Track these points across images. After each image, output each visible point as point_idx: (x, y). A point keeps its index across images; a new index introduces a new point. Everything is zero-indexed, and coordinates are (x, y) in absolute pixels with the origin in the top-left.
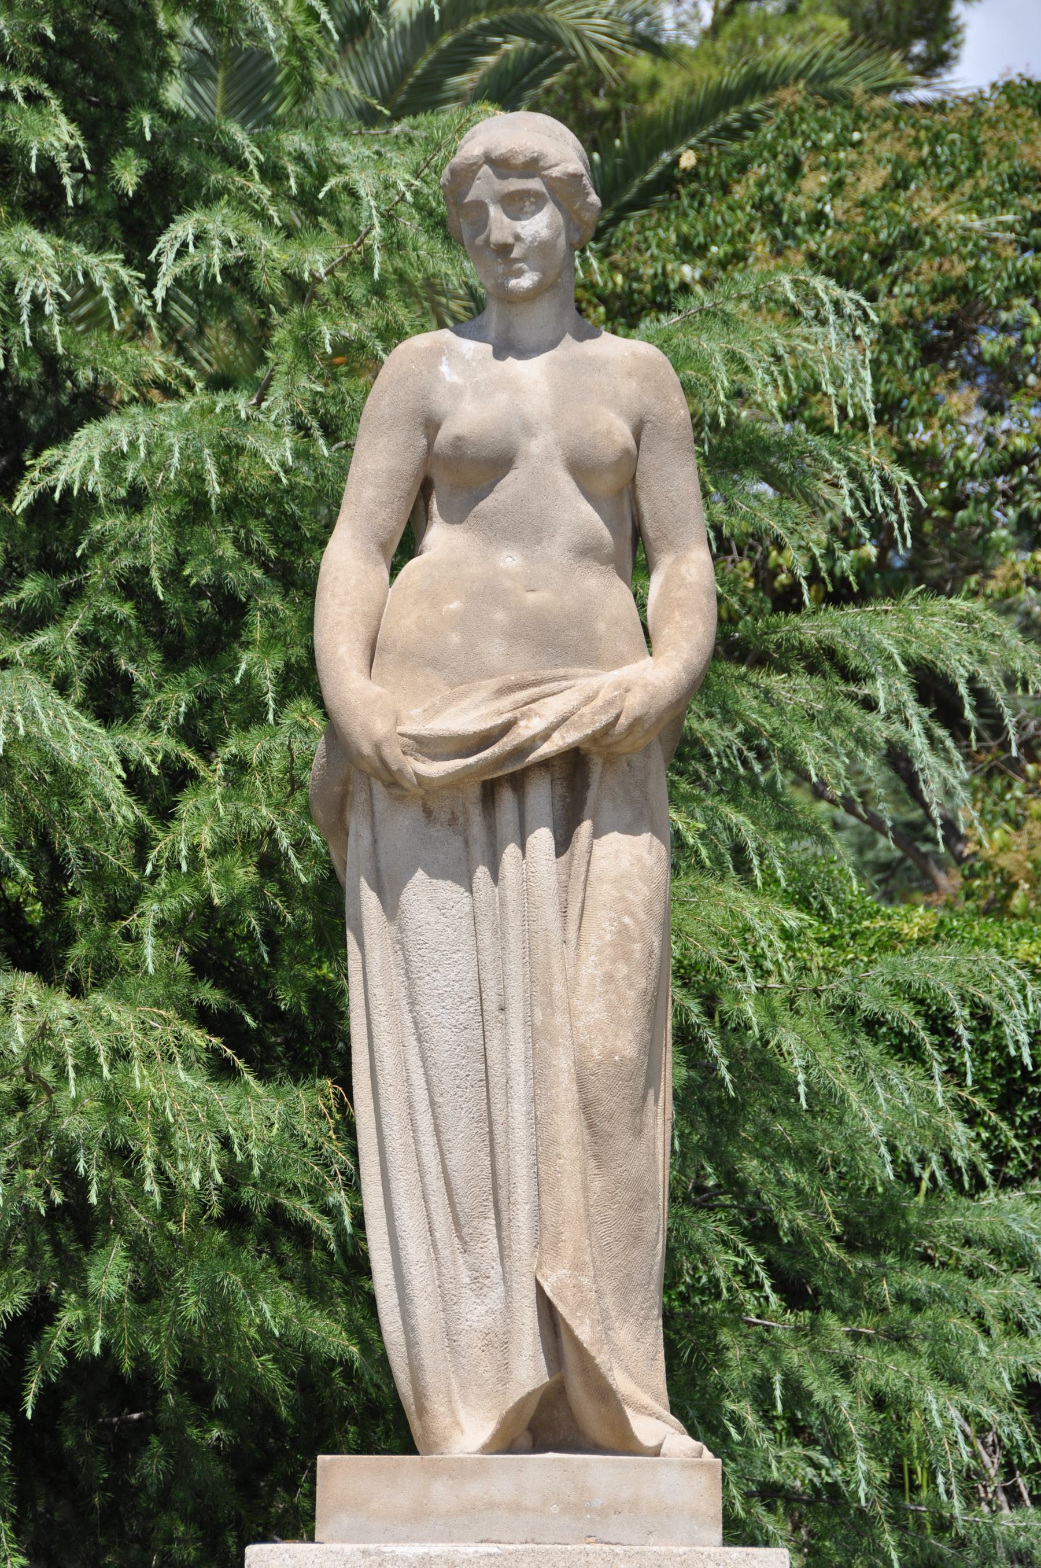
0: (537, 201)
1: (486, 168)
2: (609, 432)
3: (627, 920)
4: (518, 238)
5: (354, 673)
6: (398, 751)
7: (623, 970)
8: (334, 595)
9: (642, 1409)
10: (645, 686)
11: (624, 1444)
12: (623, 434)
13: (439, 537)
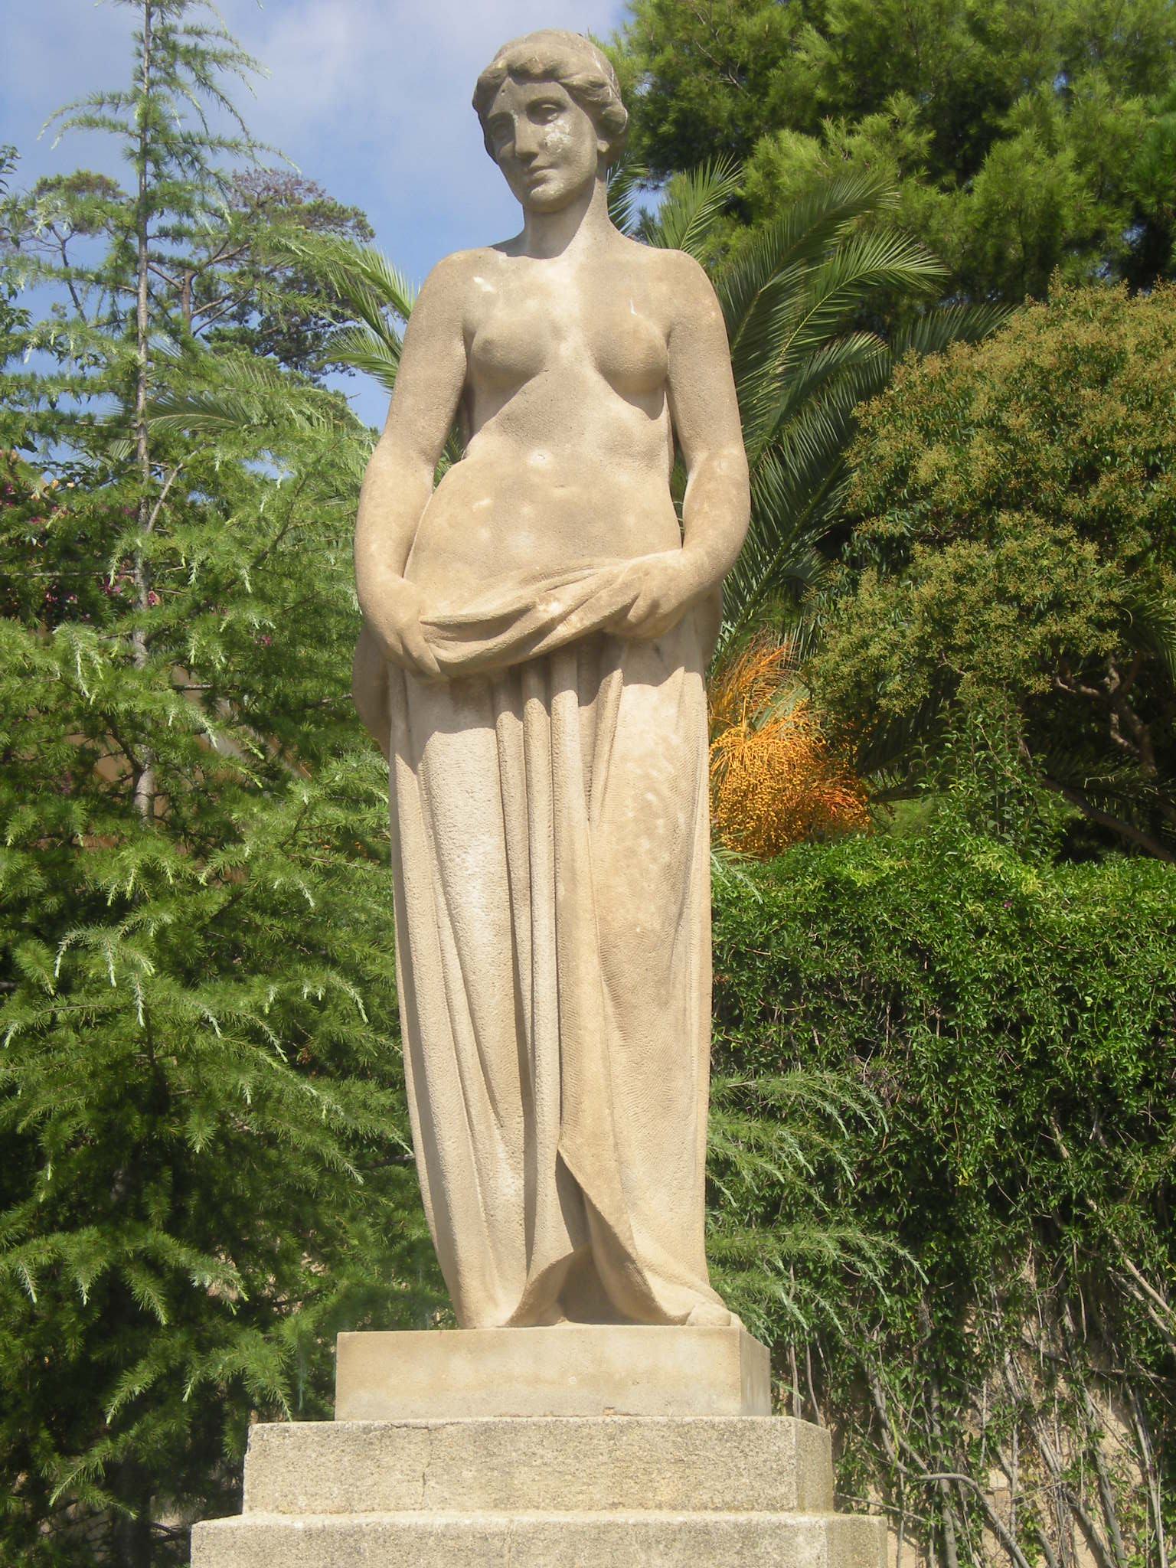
0: (560, 107)
1: (509, 80)
2: (635, 331)
3: (650, 797)
4: (543, 146)
5: (382, 568)
6: (420, 639)
7: (645, 844)
8: (371, 498)
9: (671, 1278)
10: (665, 569)
11: (642, 1310)
12: (655, 332)
13: (483, 444)
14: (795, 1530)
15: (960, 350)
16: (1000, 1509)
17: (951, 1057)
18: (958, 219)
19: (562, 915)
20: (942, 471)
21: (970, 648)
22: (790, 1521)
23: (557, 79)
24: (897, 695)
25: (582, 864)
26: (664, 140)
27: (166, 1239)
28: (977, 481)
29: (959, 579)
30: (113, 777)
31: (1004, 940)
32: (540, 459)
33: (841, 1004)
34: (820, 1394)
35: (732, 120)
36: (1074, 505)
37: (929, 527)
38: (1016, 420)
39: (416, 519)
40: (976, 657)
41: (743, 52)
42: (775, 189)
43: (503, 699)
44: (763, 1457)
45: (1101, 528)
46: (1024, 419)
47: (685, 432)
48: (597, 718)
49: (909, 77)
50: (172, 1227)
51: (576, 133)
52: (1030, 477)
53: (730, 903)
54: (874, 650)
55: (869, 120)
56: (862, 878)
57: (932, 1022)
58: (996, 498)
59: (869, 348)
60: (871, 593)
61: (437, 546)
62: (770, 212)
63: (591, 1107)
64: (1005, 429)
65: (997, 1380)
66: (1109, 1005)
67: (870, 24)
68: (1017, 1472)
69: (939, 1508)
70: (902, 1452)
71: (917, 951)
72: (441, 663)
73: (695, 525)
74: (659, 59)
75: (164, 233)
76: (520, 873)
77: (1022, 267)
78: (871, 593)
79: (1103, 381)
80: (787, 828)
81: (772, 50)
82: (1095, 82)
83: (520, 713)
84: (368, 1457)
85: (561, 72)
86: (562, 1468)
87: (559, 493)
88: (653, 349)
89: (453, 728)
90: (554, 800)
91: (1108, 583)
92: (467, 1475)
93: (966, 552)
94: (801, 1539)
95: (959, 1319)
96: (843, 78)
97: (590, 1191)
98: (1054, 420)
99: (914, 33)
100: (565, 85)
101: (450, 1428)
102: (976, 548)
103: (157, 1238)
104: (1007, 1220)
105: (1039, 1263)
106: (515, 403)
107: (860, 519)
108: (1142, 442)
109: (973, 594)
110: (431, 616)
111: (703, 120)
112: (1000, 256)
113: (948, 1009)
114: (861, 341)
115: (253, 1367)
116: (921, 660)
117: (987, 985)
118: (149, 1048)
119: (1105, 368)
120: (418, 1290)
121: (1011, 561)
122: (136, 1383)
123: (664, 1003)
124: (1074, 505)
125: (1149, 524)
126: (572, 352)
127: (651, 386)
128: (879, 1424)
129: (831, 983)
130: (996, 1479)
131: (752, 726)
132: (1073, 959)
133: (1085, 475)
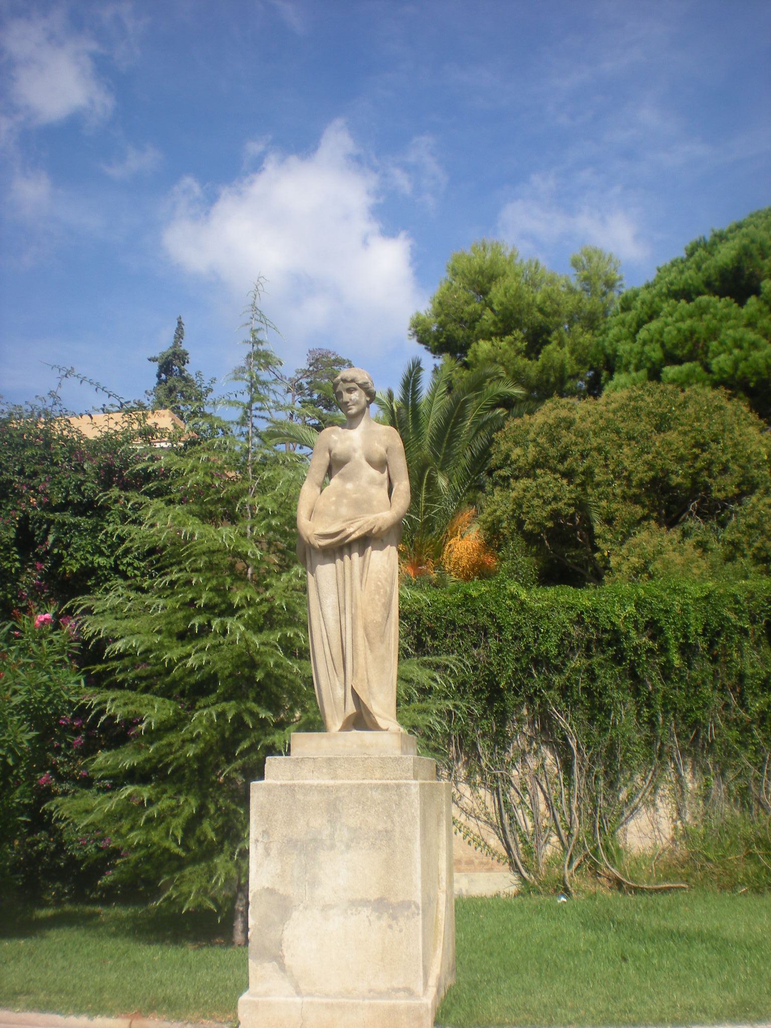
0: (355, 389)
7: (377, 597)
9: (384, 719)
11: (375, 727)
13: (335, 481)
15: (526, 417)
16: (516, 782)
17: (501, 648)
18: (534, 369)
19: (354, 617)
20: (519, 456)
21: (528, 513)
24: (505, 528)
25: (359, 604)
26: (441, 344)
27: (253, 704)
28: (530, 460)
29: (524, 491)
30: (241, 568)
31: (517, 612)
32: (349, 486)
33: (469, 632)
34: (461, 748)
35: (463, 337)
36: (560, 467)
37: (517, 473)
38: (542, 440)
40: (530, 516)
41: (466, 316)
42: (477, 359)
43: (337, 555)
45: (569, 475)
46: (544, 440)
47: (392, 477)
48: (364, 561)
49: (519, 324)
50: (254, 700)
51: (360, 396)
52: (546, 458)
53: (435, 602)
54: (498, 513)
55: (507, 337)
56: (475, 594)
57: (496, 637)
58: (536, 465)
59: (502, 412)
60: (497, 495)
61: (321, 511)
62: (475, 367)
63: (361, 672)
64: (538, 443)
65: (515, 743)
66: (548, 631)
67: (506, 309)
68: (521, 770)
69: (497, 781)
70: (487, 765)
71: (491, 616)
73: (394, 504)
74: (439, 319)
75: (257, 409)
76: (342, 605)
77: (555, 384)
78: (497, 495)
79: (568, 428)
80: (473, 570)
81: (476, 318)
82: (577, 328)
83: (342, 559)
87: (354, 496)
88: (381, 455)
90: (352, 584)
91: (570, 492)
93: (524, 482)
95: (504, 725)
96: (500, 325)
97: (360, 696)
98: (553, 440)
99: (520, 312)
102: (530, 480)
103: (252, 705)
104: (518, 696)
105: (528, 709)
106: (343, 471)
107: (495, 470)
108: (580, 448)
109: (528, 495)
110: (317, 532)
111: (454, 338)
112: (548, 381)
113: (500, 634)
114: (499, 411)
115: (277, 741)
116: (513, 517)
117: (512, 626)
118: (248, 651)
119: (569, 424)
120: (315, 724)
121: (540, 485)
122: (245, 745)
123: (382, 642)
124: (560, 467)
125: (583, 473)
126: (359, 456)
127: (381, 465)
128: (480, 757)
129: (466, 626)
130: (515, 772)
131: (462, 537)
132: (538, 617)
133: (563, 458)
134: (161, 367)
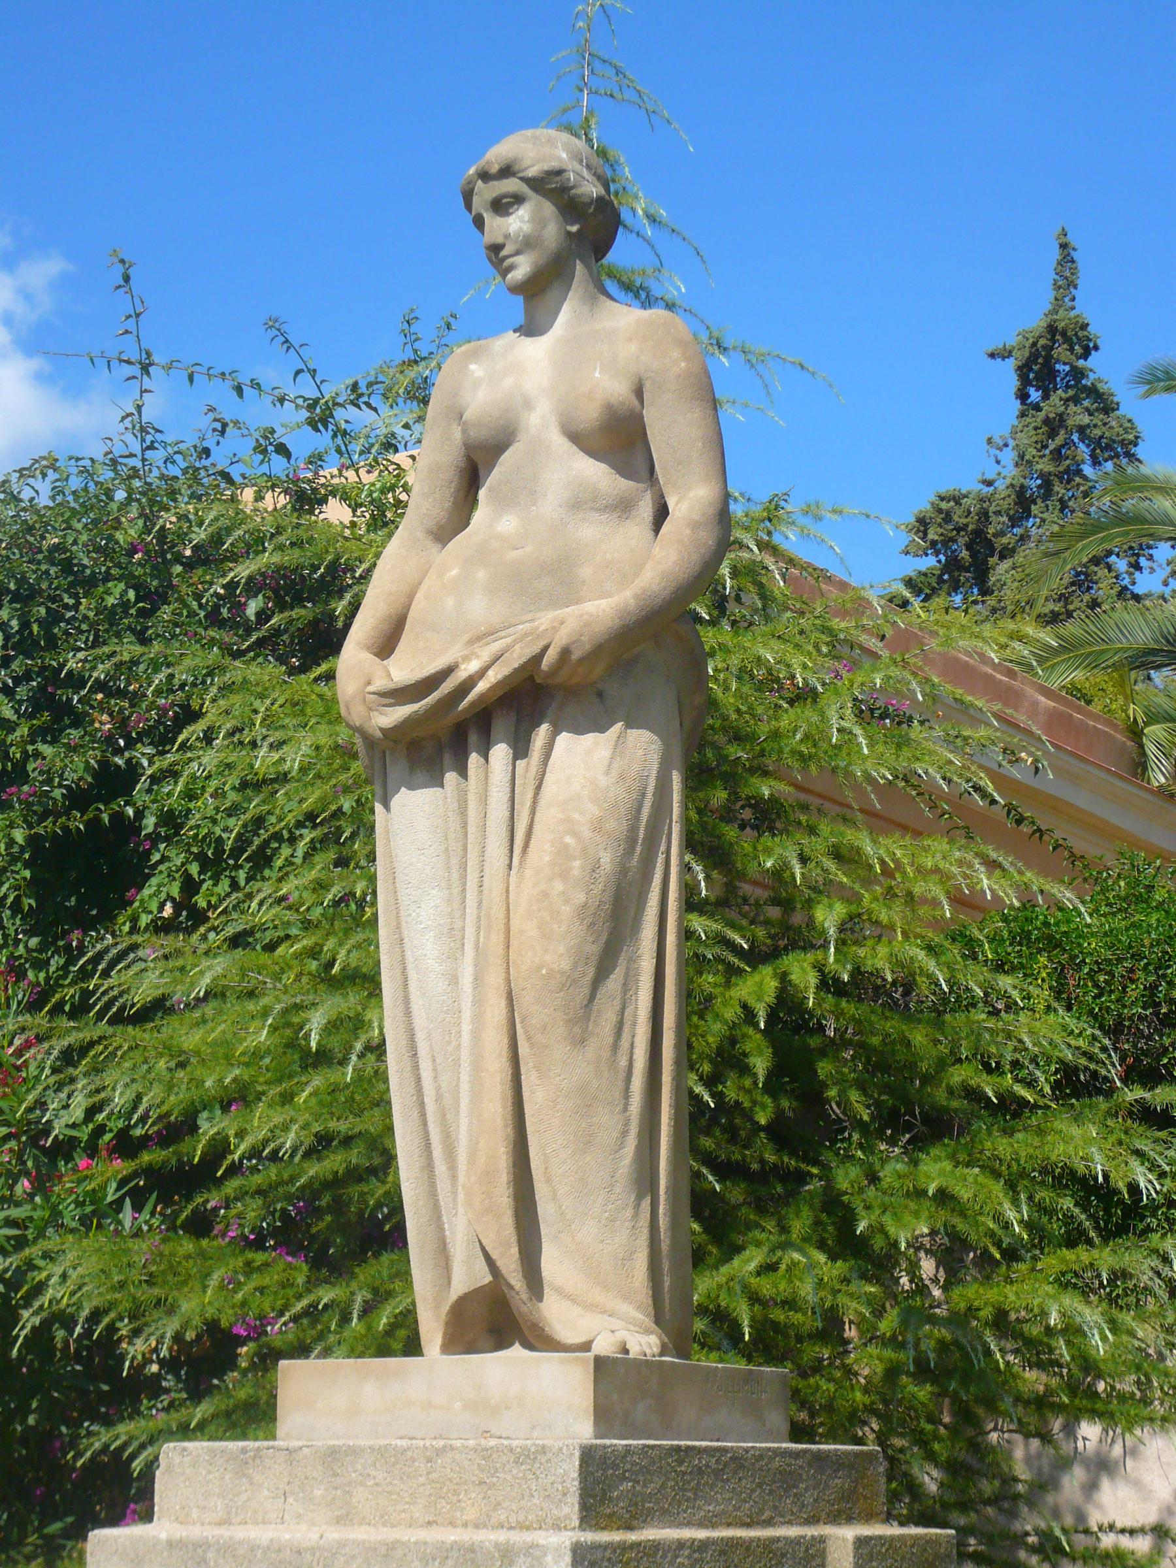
0: (518, 199)
3: (568, 839)
4: (507, 236)
7: (559, 886)
14: (544, 1550)
22: (542, 1542)
23: (514, 174)
39: (411, 597)
43: (448, 759)
44: (552, 1478)
51: (538, 221)
72: (381, 729)
84: (244, 1475)
85: (516, 168)
86: (389, 1489)
89: (412, 787)
92: (318, 1493)
94: (549, 1558)
100: (522, 179)
101: (306, 1450)
134: (1023, 371)
